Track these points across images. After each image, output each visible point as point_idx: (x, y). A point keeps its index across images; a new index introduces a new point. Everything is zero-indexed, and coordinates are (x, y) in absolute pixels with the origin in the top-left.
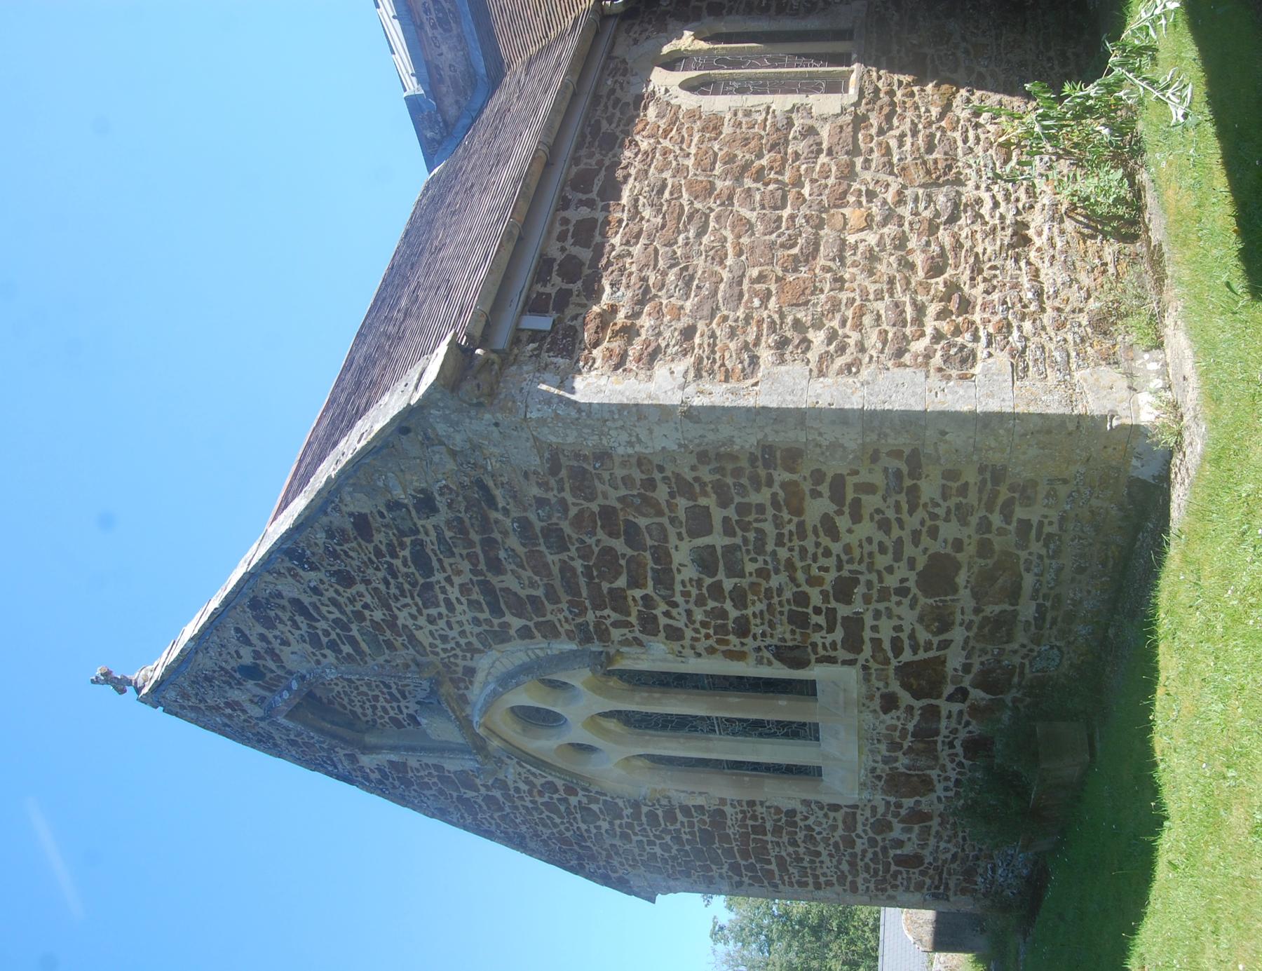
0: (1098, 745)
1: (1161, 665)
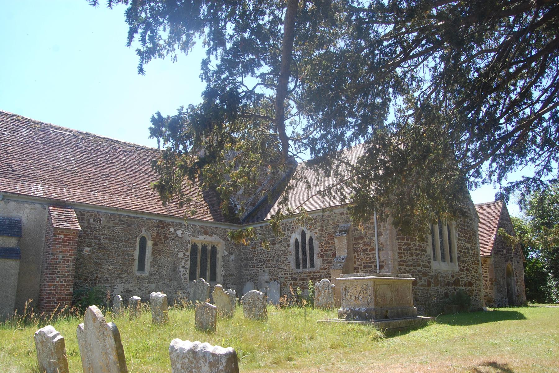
0: (113, 357)
1: (441, 325)
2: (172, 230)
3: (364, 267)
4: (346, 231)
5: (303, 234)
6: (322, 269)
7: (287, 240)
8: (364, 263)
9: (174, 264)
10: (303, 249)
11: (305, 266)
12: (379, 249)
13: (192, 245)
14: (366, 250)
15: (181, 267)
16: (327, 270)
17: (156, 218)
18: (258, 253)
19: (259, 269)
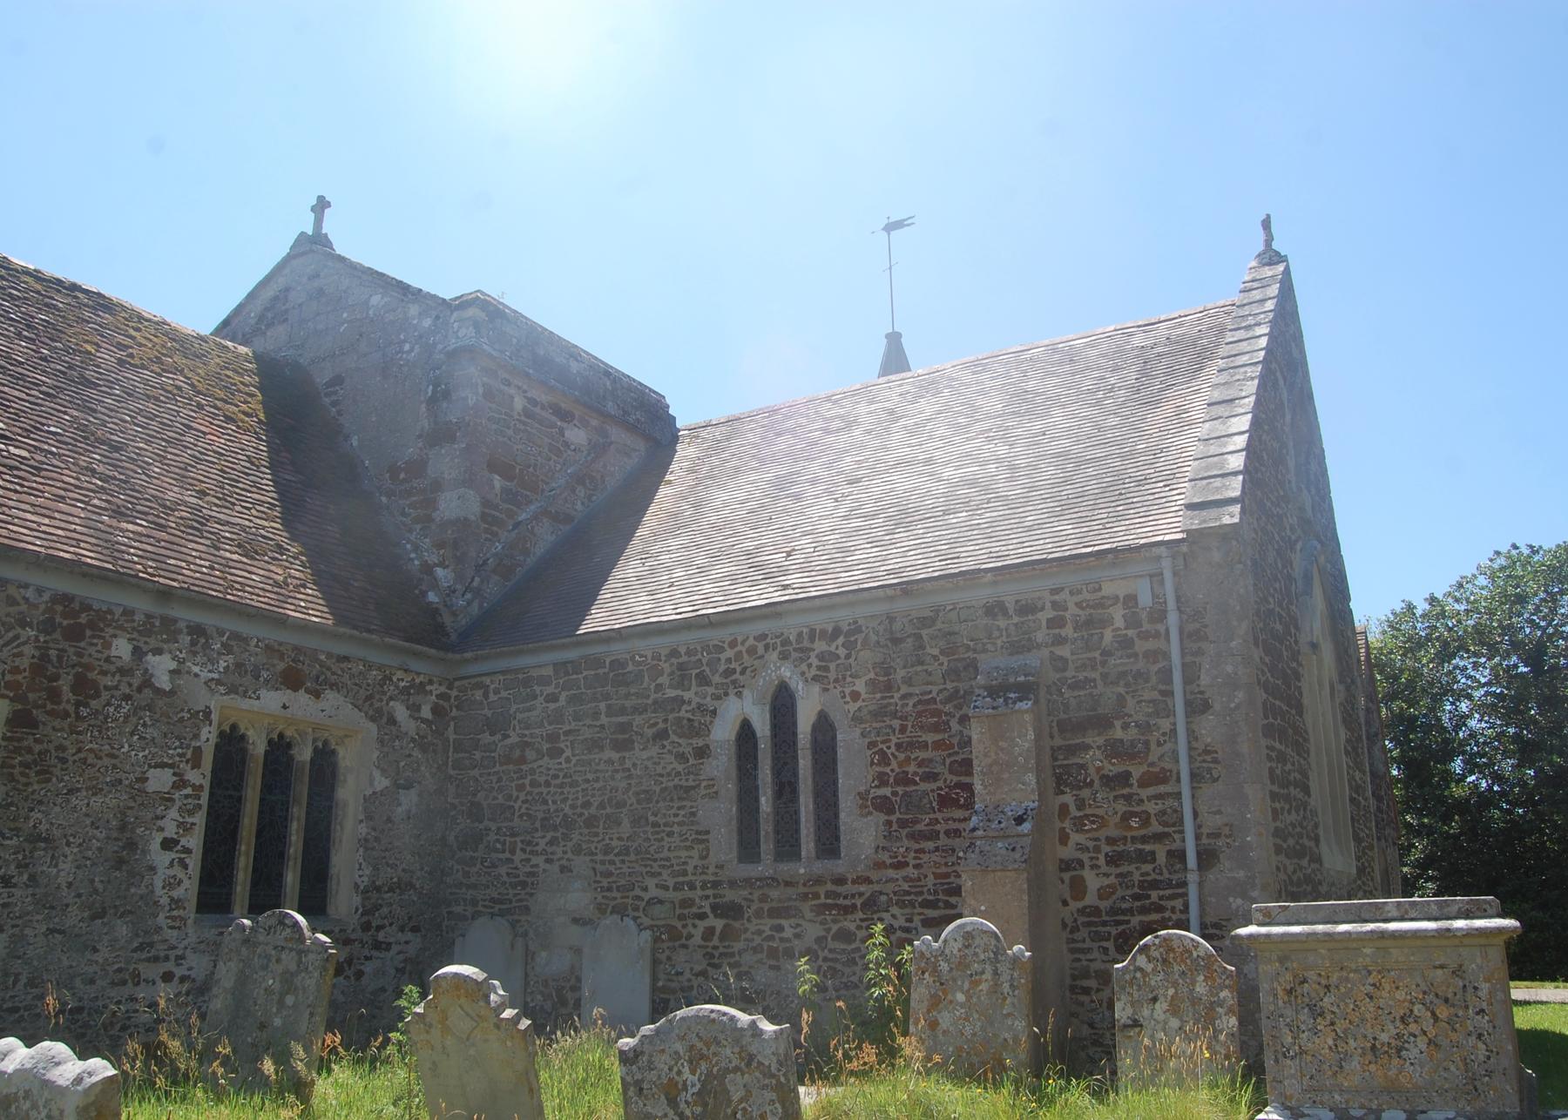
2: (122, 648)
3: (1112, 860)
4: (1025, 691)
5: (782, 705)
6: (879, 865)
7: (701, 730)
8: (1111, 841)
9: (123, 828)
10: (777, 772)
11: (788, 848)
12: (1194, 776)
13: (221, 734)
14: (1124, 778)
15: (155, 845)
16: (911, 871)
17: (36, 578)
18: (533, 784)
19: (539, 860)
